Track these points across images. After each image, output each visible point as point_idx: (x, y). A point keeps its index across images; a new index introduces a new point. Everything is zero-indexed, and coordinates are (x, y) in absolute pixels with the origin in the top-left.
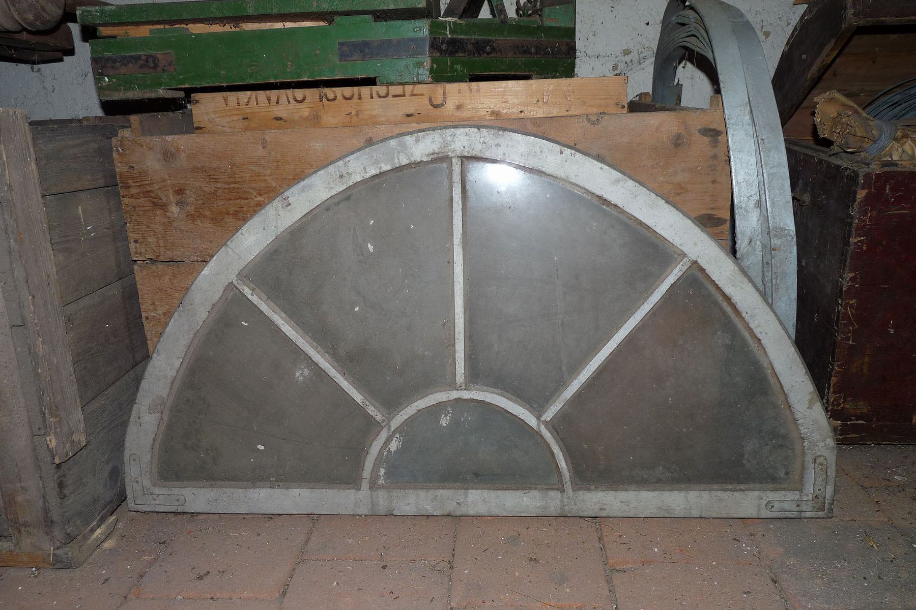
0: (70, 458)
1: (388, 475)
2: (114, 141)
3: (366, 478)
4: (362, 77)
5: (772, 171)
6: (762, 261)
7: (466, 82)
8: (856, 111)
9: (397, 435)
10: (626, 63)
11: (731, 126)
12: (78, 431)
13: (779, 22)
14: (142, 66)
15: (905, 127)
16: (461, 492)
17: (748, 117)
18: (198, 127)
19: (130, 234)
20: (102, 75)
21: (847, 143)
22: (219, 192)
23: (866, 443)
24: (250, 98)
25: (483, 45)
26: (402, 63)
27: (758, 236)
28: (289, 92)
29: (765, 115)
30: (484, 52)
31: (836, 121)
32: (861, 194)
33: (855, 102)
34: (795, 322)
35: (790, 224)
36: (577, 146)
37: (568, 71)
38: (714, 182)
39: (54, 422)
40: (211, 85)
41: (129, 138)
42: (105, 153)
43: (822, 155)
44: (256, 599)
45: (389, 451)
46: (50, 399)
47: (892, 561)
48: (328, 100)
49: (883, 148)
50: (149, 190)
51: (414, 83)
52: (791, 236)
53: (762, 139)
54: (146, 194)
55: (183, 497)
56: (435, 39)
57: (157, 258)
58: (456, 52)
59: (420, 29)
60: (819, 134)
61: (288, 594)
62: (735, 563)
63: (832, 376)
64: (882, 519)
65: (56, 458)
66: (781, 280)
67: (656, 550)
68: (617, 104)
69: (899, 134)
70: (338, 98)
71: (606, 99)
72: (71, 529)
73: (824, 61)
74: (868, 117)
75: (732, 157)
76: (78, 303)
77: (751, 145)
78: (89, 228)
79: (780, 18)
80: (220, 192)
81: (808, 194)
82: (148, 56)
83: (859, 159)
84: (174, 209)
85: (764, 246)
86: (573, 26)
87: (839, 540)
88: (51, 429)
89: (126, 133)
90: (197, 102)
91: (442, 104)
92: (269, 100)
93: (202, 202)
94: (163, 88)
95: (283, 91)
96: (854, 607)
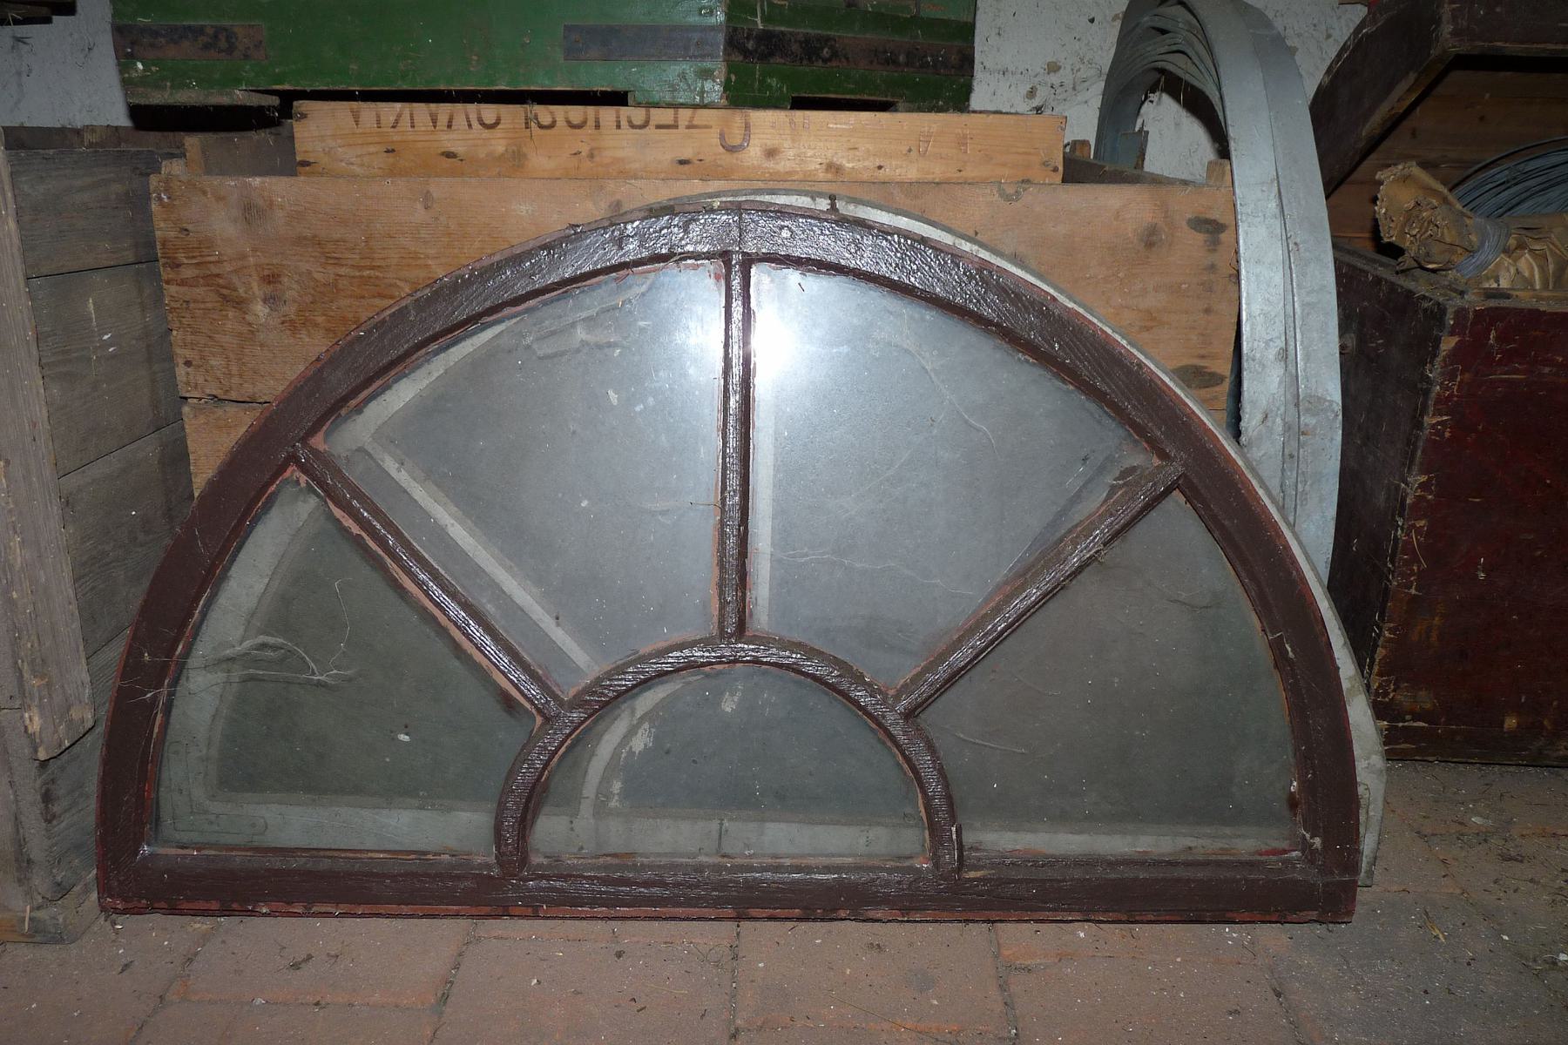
0: (65, 750)
1: (626, 794)
2: (154, 180)
3: (587, 798)
4: (604, 89)
5: (1308, 299)
6: (1283, 451)
7: (784, 108)
8: (1445, 200)
9: (646, 725)
10: (1052, 87)
11: (1244, 218)
12: (80, 702)
13: (1314, 33)
14: (206, 47)
15: (1524, 232)
16: (753, 825)
17: (1274, 204)
18: (305, 162)
19: (178, 351)
20: (132, 57)
21: (1428, 254)
22: (343, 283)
23: (1425, 758)
24: (399, 116)
25: (818, 45)
26: (673, 70)
27: (1278, 409)
28: (472, 108)
29: (1303, 202)
30: (819, 57)
31: (1410, 216)
32: (1448, 344)
33: (1435, 177)
34: (1330, 556)
35: (1332, 389)
36: (979, 237)
37: (959, 100)
38: (1208, 311)
39: (38, 687)
40: (331, 87)
41: (182, 179)
42: (138, 203)
43: (1383, 270)
44: (397, 1006)
45: (631, 753)
46: (32, 646)
47: (1469, 964)
48: (541, 127)
49: (1484, 266)
50: (214, 273)
51: (695, 107)
52: (1333, 411)
53: (1296, 244)
54: (210, 279)
55: (262, 821)
56: (735, 30)
57: (225, 394)
58: (772, 54)
59: (712, 12)
60: (1382, 235)
61: (452, 999)
62: (1212, 960)
63: (1378, 646)
64: (1451, 890)
65: (40, 749)
66: (1311, 485)
67: (1082, 935)
68: (1045, 164)
69: (1512, 242)
70: (558, 124)
71: (1026, 153)
72: (63, 874)
73: (1393, 108)
74: (1465, 210)
75: (1243, 272)
76: (84, 472)
77: (1277, 252)
78: (106, 337)
79: (1315, 26)
80: (345, 282)
81: (1353, 335)
82: (219, 30)
83: (1446, 283)
84: (260, 310)
85: (1287, 428)
86: (970, 20)
87: (1382, 925)
88: (32, 699)
89: (174, 168)
90: (304, 116)
91: (741, 146)
92: (434, 122)
93: (311, 299)
94: (244, 88)
95: (459, 106)
96: (1408, 1041)
